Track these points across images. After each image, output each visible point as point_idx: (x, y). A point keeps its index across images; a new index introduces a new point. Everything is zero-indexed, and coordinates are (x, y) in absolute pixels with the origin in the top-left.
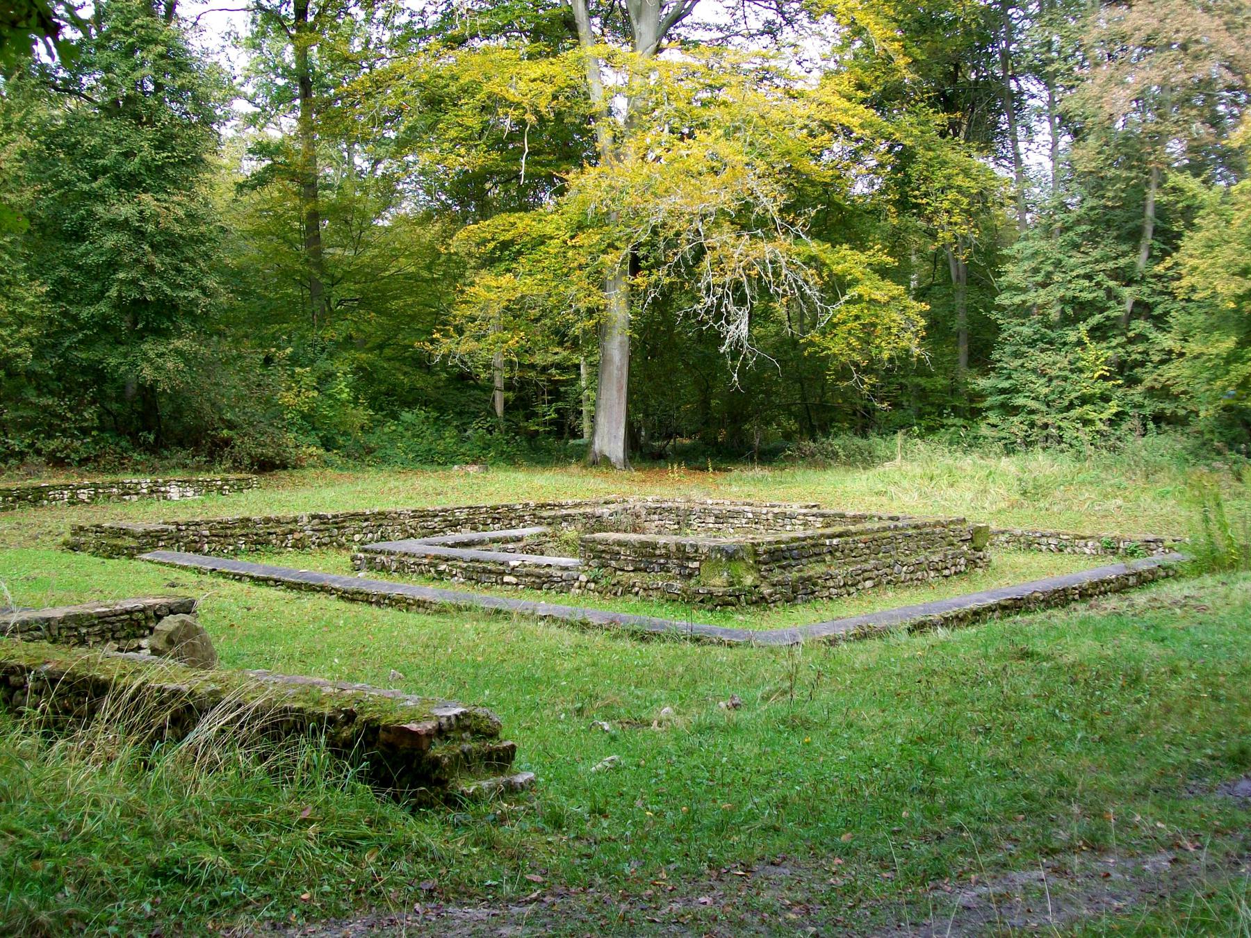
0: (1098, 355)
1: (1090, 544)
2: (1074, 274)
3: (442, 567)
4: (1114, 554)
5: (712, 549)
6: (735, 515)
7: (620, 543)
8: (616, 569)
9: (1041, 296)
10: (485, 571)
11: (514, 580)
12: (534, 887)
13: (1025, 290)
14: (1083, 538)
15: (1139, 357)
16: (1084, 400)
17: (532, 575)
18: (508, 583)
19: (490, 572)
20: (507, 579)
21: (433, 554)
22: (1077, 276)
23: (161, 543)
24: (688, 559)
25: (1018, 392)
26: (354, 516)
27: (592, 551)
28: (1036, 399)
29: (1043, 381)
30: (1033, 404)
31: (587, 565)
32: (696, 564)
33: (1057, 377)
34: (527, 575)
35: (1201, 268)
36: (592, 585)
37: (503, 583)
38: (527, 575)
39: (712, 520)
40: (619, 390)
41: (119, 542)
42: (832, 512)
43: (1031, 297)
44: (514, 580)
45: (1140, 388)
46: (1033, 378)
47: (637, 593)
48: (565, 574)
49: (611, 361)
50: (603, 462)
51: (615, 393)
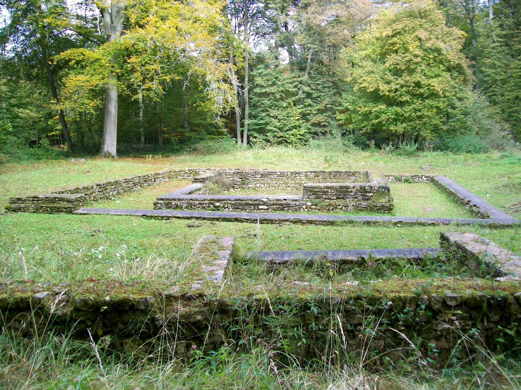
0: (297, 110)
1: (390, 178)
2: (286, 82)
3: (217, 204)
4: (400, 181)
5: (380, 187)
6: (270, 174)
7: (327, 188)
8: (325, 199)
9: (273, 89)
10: (246, 204)
11: (266, 207)
12: (387, 342)
13: (264, 87)
14: (387, 176)
15: (309, 112)
16: (295, 127)
17: (277, 204)
18: (261, 209)
19: (250, 204)
20: (260, 207)
21: (209, 198)
22: (287, 83)
23: (81, 204)
24: (367, 192)
25: (268, 124)
26: (109, 183)
27: (311, 191)
28: (275, 127)
29: (277, 120)
30: (275, 129)
31: (308, 198)
32: (371, 194)
33: (282, 119)
34: (274, 205)
35: (368, 81)
36: (314, 207)
37: (259, 209)
38: (274, 205)
39: (260, 176)
40: (114, 126)
41: (55, 205)
42: (319, 170)
43: (268, 90)
44: (266, 207)
45: (310, 123)
46: (273, 119)
47: (341, 209)
48: (297, 203)
49: (111, 113)
50: (108, 155)
51: (113, 127)
